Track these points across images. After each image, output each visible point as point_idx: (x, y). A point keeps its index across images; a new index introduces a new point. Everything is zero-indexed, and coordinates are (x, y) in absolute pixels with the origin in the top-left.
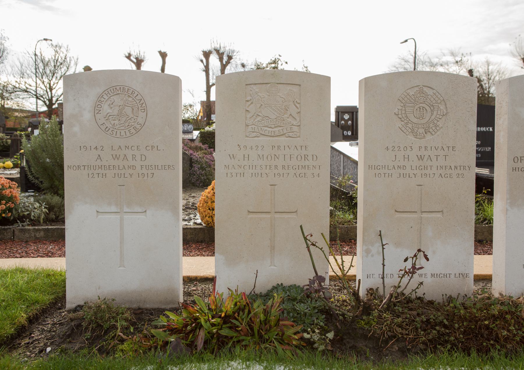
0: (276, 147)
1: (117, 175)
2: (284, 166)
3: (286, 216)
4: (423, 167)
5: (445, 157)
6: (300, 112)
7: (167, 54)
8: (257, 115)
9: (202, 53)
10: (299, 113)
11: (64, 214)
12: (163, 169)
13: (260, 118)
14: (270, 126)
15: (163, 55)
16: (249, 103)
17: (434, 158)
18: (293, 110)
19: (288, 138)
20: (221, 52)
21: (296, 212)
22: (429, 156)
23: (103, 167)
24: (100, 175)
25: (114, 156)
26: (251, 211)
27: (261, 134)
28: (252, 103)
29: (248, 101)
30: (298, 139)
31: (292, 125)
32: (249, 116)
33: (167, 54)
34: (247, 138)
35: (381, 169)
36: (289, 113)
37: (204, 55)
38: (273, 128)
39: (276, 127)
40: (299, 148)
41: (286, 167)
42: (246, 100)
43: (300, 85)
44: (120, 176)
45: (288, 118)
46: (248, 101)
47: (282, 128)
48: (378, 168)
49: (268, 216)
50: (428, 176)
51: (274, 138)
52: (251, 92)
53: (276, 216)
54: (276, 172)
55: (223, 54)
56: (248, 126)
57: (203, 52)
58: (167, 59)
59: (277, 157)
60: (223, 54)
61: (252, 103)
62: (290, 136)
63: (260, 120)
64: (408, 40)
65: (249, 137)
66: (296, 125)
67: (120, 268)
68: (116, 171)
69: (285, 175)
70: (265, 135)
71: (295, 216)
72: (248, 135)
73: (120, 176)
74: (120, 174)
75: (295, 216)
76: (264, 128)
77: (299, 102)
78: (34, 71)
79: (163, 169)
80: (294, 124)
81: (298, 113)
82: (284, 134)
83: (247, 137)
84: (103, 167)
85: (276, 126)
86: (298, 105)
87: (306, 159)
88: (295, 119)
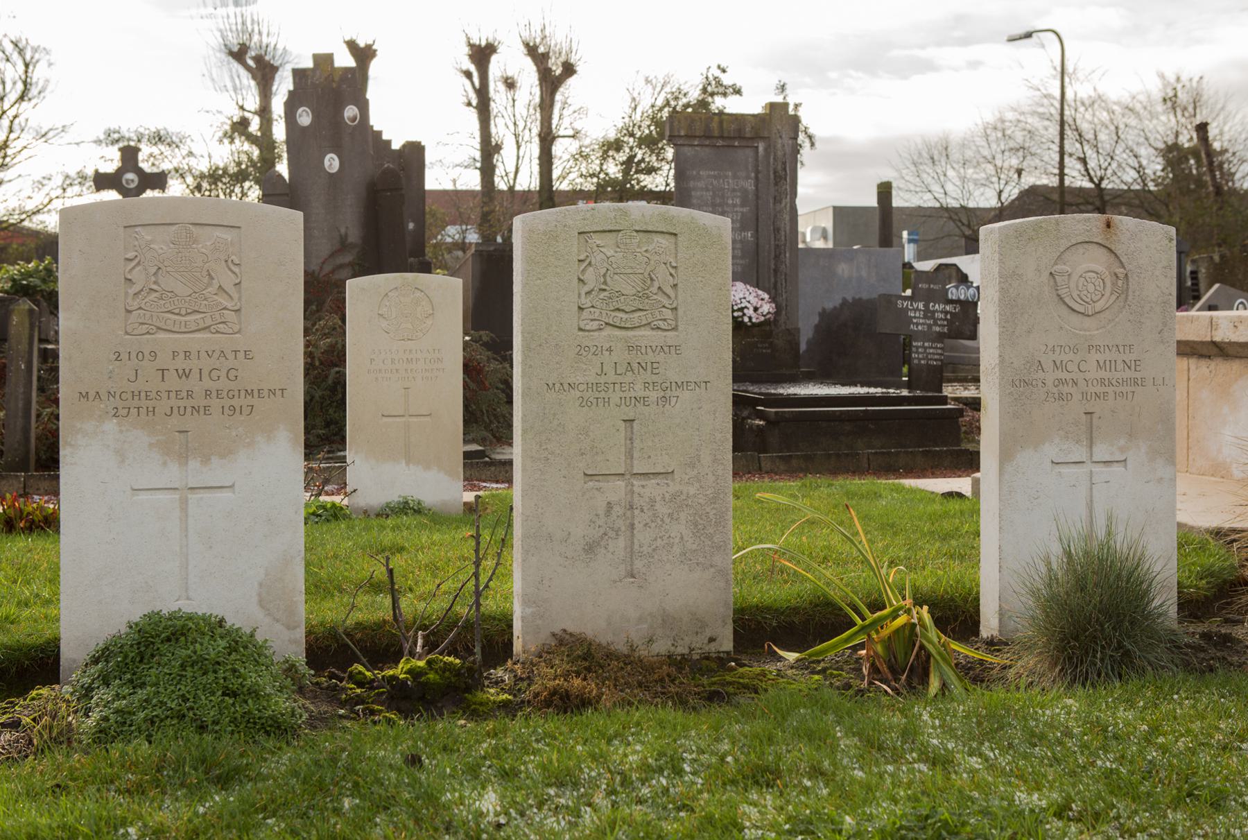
1: (175, 410)
4: (236, 393)
6: (240, 283)
7: (375, 51)
8: (151, 289)
9: (466, 50)
10: (675, 285)
13: (606, 294)
14: (177, 311)
16: (133, 264)
19: (654, 333)
20: (541, 50)
24: (143, 411)
25: (181, 372)
27: (159, 328)
28: (138, 264)
29: (131, 260)
31: (225, 308)
32: (131, 291)
33: (375, 51)
34: (127, 337)
35: (236, 396)
36: (215, 283)
37: (471, 57)
42: (127, 256)
43: (675, 235)
44: (182, 412)
55: (545, 56)
57: (471, 46)
60: (545, 56)
64: (1034, 35)
68: (173, 402)
69: (246, 410)
73: (182, 412)
74: (182, 410)
80: (667, 305)
82: (649, 324)
83: (580, 329)
85: (189, 311)
86: (236, 269)
88: (230, 296)
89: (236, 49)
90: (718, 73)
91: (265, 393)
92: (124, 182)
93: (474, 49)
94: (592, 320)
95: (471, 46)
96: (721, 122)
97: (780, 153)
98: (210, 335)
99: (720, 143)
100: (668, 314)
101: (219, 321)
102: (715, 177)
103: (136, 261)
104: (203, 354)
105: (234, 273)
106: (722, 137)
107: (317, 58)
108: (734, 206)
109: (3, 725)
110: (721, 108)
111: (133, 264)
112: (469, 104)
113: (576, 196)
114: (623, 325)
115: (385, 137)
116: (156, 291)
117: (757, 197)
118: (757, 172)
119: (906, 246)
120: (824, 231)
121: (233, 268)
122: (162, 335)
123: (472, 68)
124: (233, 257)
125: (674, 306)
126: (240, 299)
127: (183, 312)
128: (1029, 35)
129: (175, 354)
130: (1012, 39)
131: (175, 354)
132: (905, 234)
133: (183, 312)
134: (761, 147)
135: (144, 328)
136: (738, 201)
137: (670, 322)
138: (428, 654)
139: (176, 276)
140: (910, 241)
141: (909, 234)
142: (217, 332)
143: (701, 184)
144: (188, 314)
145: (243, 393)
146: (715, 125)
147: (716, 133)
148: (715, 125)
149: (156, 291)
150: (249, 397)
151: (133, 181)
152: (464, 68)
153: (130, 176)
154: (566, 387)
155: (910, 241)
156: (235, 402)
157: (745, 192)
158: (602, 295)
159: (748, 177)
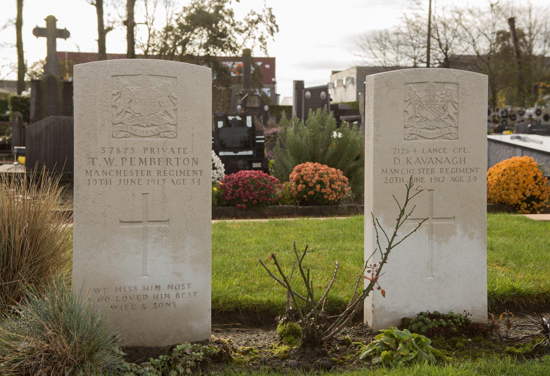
0: (149, 150)
2: (159, 172)
3: (444, 222)
4: (175, 173)
5: (178, 160)
11: (364, 226)
12: (465, 172)
16: (117, 97)
17: (174, 162)
18: (451, 110)
21: (168, 220)
22: (140, 158)
23: (186, 172)
26: (124, 221)
30: (456, 140)
31: (451, 126)
38: (145, 128)
39: (149, 126)
40: (176, 151)
41: (162, 172)
43: (176, 78)
45: (163, 115)
46: (406, 101)
47: (157, 127)
48: (453, 172)
49: (140, 226)
50: (156, 182)
52: (118, 85)
54: (433, 176)
56: (406, 128)
59: (196, 162)
61: (120, 97)
62: (166, 136)
63: (130, 118)
65: (408, 140)
66: (454, 126)
67: (427, 278)
69: (161, 182)
70: (422, 137)
71: (452, 223)
72: (407, 138)
74: (126, 181)
75: (452, 223)
76: (135, 127)
77: (175, 97)
78: (374, 56)
79: (465, 172)
80: (453, 125)
81: (175, 110)
82: (159, 133)
83: (405, 139)
84: (186, 172)
87: (169, 163)
94: (411, 134)
98: (162, 139)
100: (453, 130)
101: (448, 132)
103: (410, 101)
105: (174, 104)
110: (230, 10)
111: (117, 97)
112: (92, 4)
113: (140, 56)
114: (141, 134)
116: (419, 117)
120: (353, 79)
121: (455, 105)
124: (173, 94)
125: (456, 125)
126: (177, 117)
127: (145, 125)
129: (145, 149)
131: (145, 149)
133: (145, 125)
135: (122, 134)
137: (172, 133)
138: (429, 334)
139: (427, 108)
142: (165, 137)
144: (148, 126)
149: (419, 117)
150: (182, 175)
154: (393, 171)
158: (128, 115)
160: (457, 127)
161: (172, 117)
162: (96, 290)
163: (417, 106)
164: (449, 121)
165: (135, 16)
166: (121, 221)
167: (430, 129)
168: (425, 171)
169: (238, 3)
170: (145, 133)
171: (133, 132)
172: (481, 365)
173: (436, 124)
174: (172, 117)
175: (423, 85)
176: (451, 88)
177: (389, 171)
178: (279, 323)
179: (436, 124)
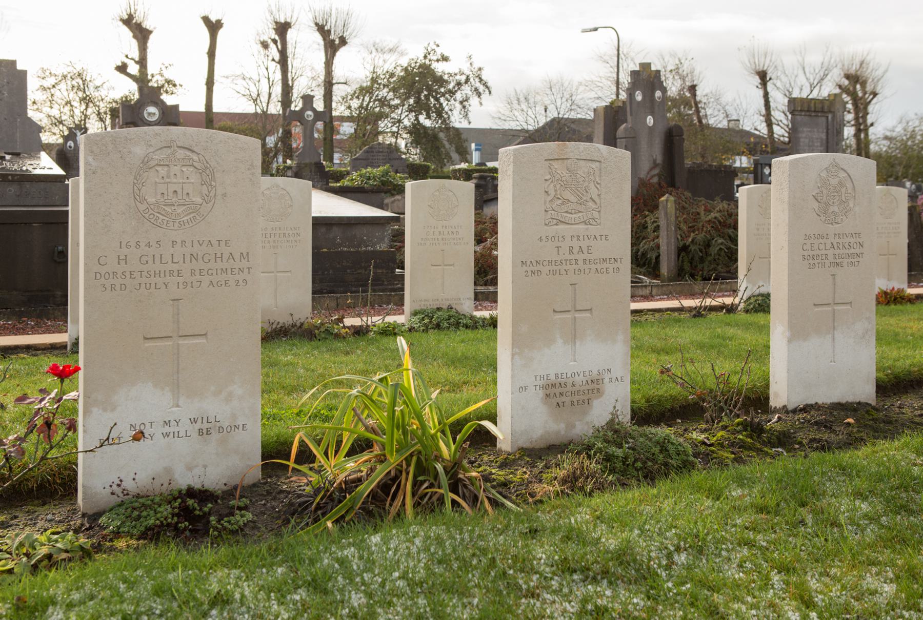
1: (143, 286)
4: (598, 261)
13: (560, 201)
15: (214, 27)
21: (205, 335)
49: (169, 343)
51: (572, 226)
53: (147, 345)
55: (329, 31)
57: (276, 23)
58: (221, 34)
60: (329, 31)
83: (546, 225)
89: (126, 17)
90: (434, 47)
91: (236, 271)
92: (146, 116)
93: (278, 25)
95: (276, 23)
96: (815, 104)
97: (838, 120)
99: (813, 114)
100: (596, 214)
102: (810, 131)
104: (196, 243)
106: (815, 111)
107: (642, 65)
108: (817, 146)
109: (3, 572)
115: (20, 67)
117: (827, 142)
118: (828, 129)
119: (474, 152)
122: (562, 227)
123: (277, 38)
128: (596, 29)
130: (585, 31)
132: (473, 146)
134: (830, 116)
136: (819, 144)
140: (476, 150)
141: (476, 145)
143: (804, 135)
144: (575, 213)
145: (219, 272)
146: (812, 105)
147: (813, 109)
148: (812, 105)
151: (154, 114)
152: (273, 38)
153: (152, 109)
155: (476, 150)
156: (599, 267)
157: (822, 139)
159: (823, 132)
160: (599, 212)
161: (596, 203)
162: (192, 420)
163: (558, 186)
164: (591, 204)
165: (324, 60)
166: (146, 338)
167: (571, 213)
168: (568, 262)
169: (203, 15)
170: (573, 220)
171: (563, 220)
172: (25, 589)
173: (579, 208)
174: (596, 203)
175: (566, 161)
176: (594, 167)
177: (528, 263)
178: (433, 437)
179: (579, 208)
